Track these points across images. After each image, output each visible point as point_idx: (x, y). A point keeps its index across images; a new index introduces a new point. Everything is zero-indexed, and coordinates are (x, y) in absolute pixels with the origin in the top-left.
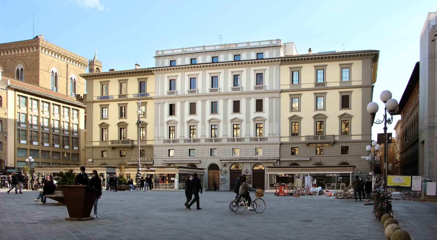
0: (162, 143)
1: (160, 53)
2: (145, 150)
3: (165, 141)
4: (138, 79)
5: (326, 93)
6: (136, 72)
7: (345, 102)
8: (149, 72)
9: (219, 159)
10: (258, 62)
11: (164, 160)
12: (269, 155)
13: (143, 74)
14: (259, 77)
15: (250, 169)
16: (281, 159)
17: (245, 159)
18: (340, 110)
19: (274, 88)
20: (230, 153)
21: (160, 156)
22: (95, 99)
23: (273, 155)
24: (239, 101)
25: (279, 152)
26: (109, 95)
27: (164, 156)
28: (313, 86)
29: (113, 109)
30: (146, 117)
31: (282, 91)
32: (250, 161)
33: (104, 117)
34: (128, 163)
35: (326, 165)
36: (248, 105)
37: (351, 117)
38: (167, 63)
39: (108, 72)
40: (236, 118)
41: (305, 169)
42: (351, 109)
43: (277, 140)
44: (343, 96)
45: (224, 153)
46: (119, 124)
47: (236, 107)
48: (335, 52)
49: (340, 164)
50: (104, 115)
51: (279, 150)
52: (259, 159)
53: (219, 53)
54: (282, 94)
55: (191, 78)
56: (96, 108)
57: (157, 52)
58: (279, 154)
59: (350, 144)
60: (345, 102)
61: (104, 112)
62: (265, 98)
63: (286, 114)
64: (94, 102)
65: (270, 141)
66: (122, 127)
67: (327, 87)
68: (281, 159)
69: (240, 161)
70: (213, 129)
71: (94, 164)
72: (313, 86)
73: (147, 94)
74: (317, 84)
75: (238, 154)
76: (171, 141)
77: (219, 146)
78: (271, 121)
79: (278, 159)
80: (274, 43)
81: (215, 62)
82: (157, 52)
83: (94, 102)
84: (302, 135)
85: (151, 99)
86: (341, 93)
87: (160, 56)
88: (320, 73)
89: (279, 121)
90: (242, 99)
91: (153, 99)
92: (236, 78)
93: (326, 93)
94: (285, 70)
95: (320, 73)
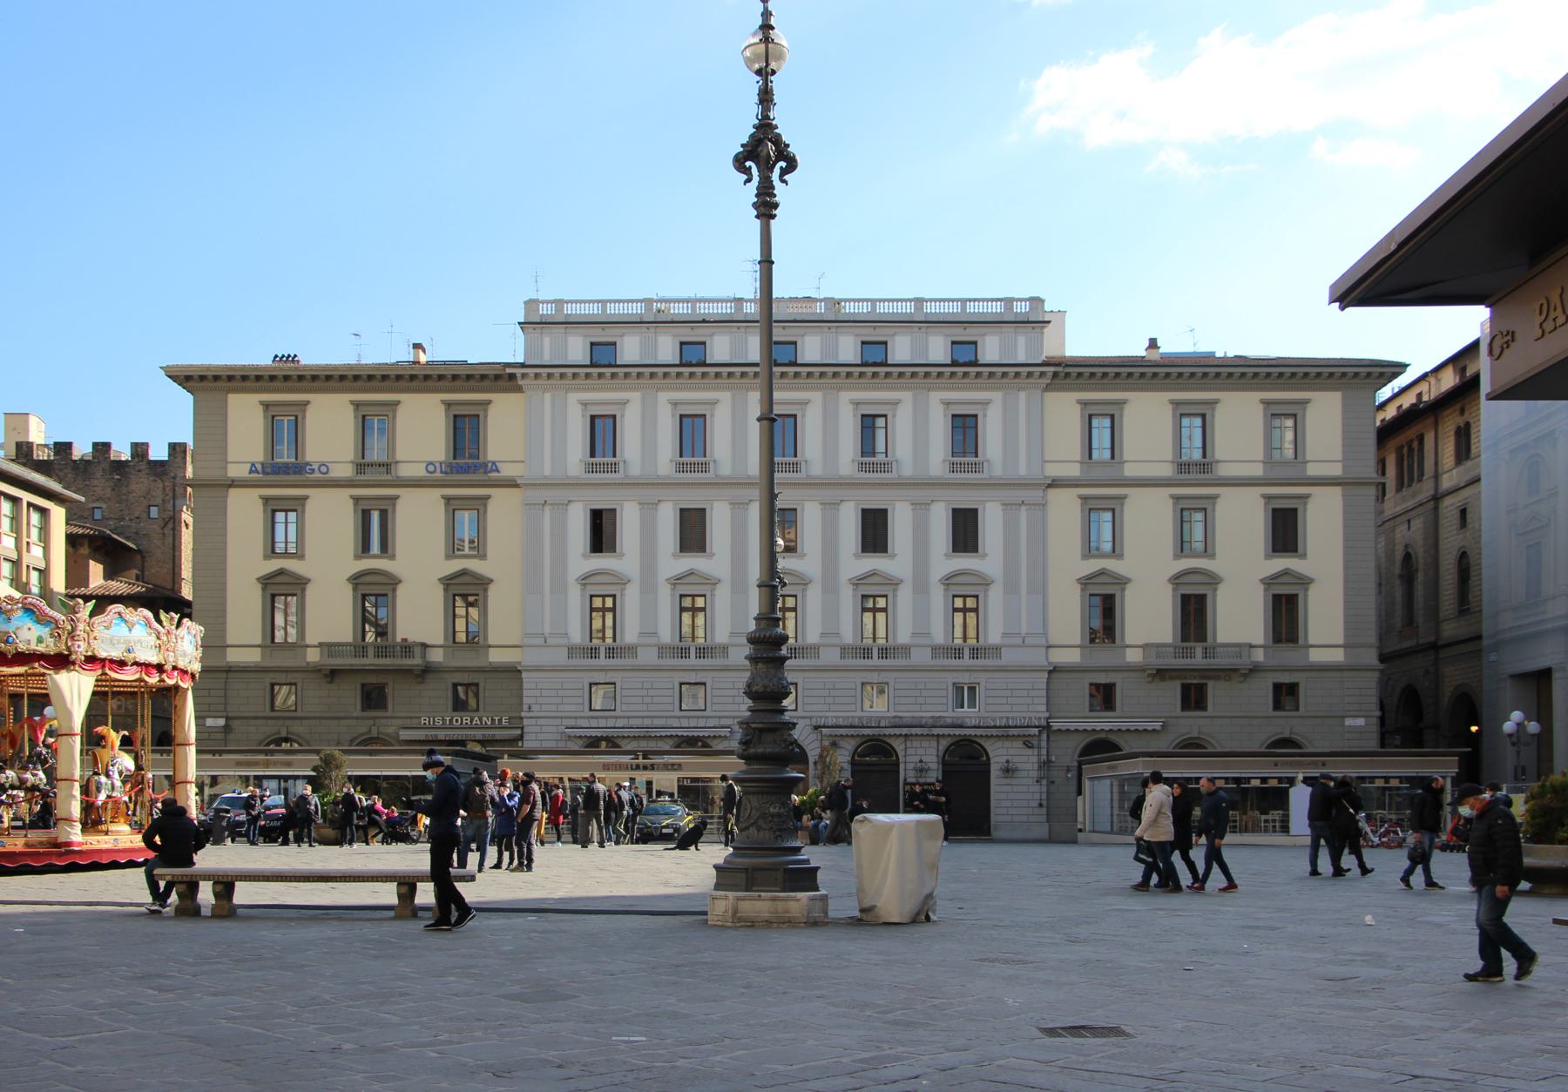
0: (561, 658)
1: (546, 310)
2: (473, 682)
3: (572, 651)
4: (448, 405)
5: (1213, 498)
6: (413, 377)
7: (1285, 531)
8: (501, 378)
9: (808, 722)
10: (600, 375)
11: (572, 722)
12: (1007, 708)
13: (468, 386)
14: (965, 428)
15: (934, 759)
16: (1055, 725)
17: (915, 722)
18: (1267, 557)
19: (547, 472)
20: (851, 700)
21: (551, 707)
22: (237, 471)
23: (554, 708)
24: (885, 511)
25: (1044, 700)
26: (308, 458)
27: (568, 708)
28: (1167, 471)
29: (329, 522)
30: (483, 557)
31: (1055, 484)
32: (936, 731)
33: (280, 548)
34: (405, 735)
35: (1219, 750)
36: (919, 531)
37: (1305, 582)
38: (576, 349)
39: (266, 368)
40: (691, 573)
41: (1286, 763)
42: (1304, 556)
43: (1037, 658)
44: (1274, 510)
45: (830, 700)
46: (356, 580)
47: (874, 530)
48: (1211, 355)
49: (1269, 747)
50: (280, 536)
51: (1044, 693)
52: (969, 722)
53: (802, 331)
54: (1052, 492)
55: (593, 418)
56: (244, 510)
57: (531, 304)
58: (1044, 708)
59: (895, 674)
60: (1285, 531)
61: (280, 529)
62: (988, 505)
63: (1068, 567)
64: (234, 484)
65: (1008, 657)
66: (374, 593)
67: (1220, 478)
68: (1055, 725)
69: (897, 731)
70: (597, 610)
71: (230, 736)
72: (1167, 471)
73: (485, 467)
74: (1183, 466)
75: (878, 707)
76: (603, 648)
77: (807, 674)
78: (1011, 587)
79: (1043, 723)
80: (1021, 308)
81: (693, 360)
82: (531, 304)
83: (234, 484)
84: (1128, 642)
85: (511, 484)
86: (1268, 498)
87: (545, 323)
88: (1101, 427)
89: (1040, 588)
90: (716, 504)
91: (517, 486)
92: (868, 423)
93: (488, 497)
94: (1064, 409)
95: (1101, 427)
